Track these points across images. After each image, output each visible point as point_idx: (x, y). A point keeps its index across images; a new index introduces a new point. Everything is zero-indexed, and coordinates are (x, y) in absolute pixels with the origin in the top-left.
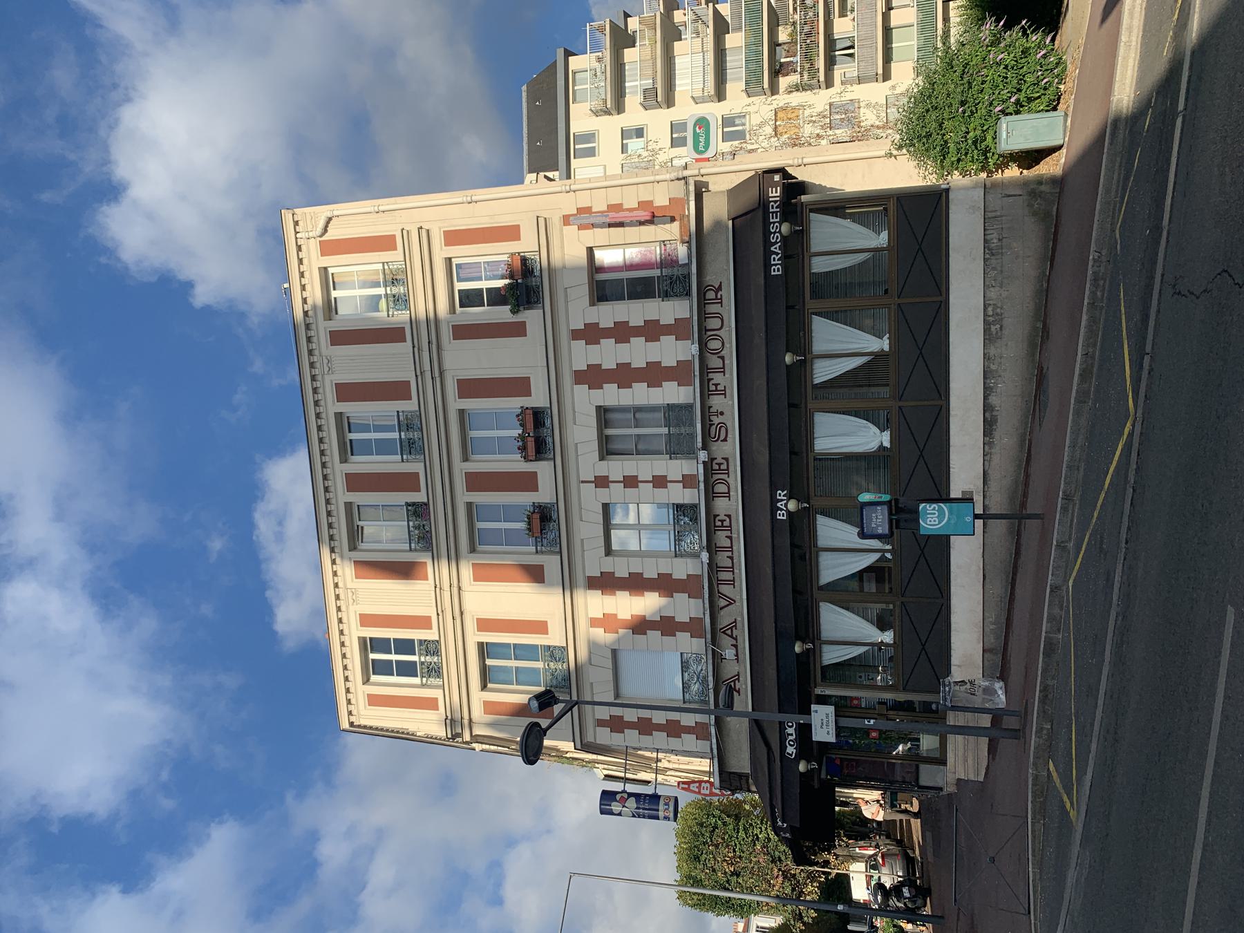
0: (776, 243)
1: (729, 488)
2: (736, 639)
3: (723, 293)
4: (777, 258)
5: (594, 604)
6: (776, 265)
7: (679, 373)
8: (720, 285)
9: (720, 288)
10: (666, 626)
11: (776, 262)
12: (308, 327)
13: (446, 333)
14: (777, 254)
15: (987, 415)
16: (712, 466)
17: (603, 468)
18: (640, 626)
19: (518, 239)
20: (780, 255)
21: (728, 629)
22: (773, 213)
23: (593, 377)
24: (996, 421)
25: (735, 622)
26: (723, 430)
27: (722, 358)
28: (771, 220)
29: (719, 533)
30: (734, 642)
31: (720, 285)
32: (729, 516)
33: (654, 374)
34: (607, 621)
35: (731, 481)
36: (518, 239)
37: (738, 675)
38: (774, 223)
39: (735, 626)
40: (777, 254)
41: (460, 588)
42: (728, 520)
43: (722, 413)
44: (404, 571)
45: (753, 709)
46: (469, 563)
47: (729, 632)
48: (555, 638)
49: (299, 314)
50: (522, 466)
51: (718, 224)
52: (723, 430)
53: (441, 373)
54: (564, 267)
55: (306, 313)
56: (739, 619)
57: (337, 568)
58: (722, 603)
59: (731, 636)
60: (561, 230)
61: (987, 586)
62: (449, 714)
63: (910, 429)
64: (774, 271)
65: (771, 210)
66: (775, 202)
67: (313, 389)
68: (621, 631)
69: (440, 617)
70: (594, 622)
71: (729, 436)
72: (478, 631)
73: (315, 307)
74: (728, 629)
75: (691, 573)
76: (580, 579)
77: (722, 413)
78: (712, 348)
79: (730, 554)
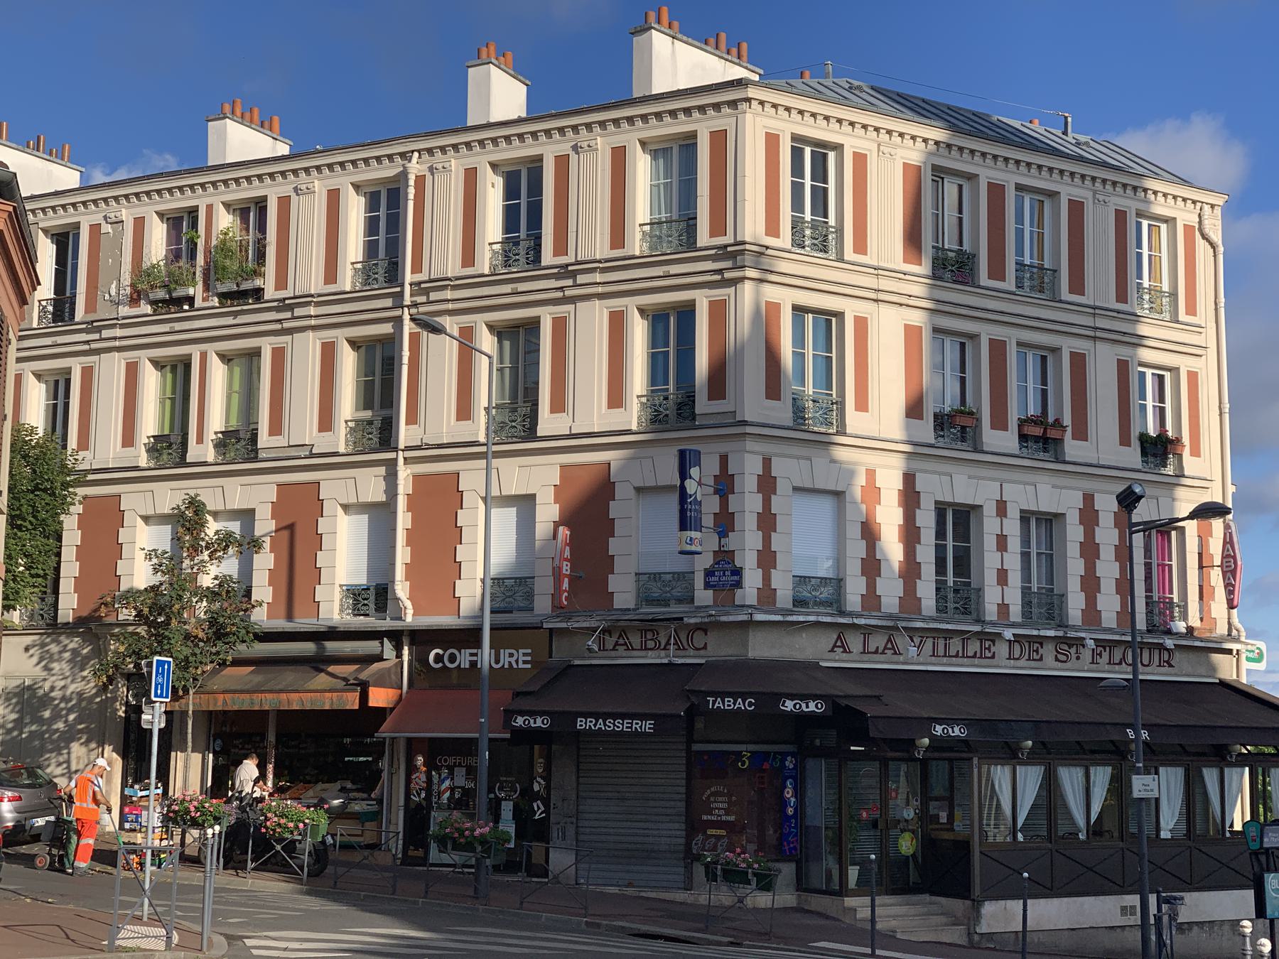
0: (605, 725)
1: (1018, 659)
2: (883, 653)
3: (1166, 669)
4: (637, 726)
5: (890, 481)
6: (586, 723)
7: (1091, 613)
8: (1173, 666)
9: (1171, 666)
10: (872, 566)
11: (588, 724)
12: (1135, 188)
13: (1124, 352)
14: (595, 725)
15: (1186, 926)
16: (988, 640)
17: (1013, 513)
18: (870, 533)
19: (857, 409)
20: (593, 728)
21: (842, 642)
22: (632, 723)
23: (1089, 516)
24: (1182, 934)
25: (900, 654)
26: (1064, 658)
27: (1120, 663)
28: (625, 721)
29: (978, 644)
30: (880, 651)
31: (1173, 666)
32: (993, 657)
33: (1091, 584)
34: (873, 492)
35: (1022, 663)
36: (857, 409)
37: (850, 652)
38: (623, 724)
39: (628, 649)
40: (595, 725)
41: (901, 305)
42: (989, 655)
43: (1078, 658)
44: (913, 238)
45: (1141, 680)
46: (923, 323)
47: (839, 643)
48: (854, 421)
49: (1151, 184)
50: (1014, 416)
51: (1213, 669)
52: (1064, 658)
53: (1095, 338)
54: (1174, 500)
55: (1145, 190)
56: (901, 658)
57: (920, 144)
58: (917, 640)
59: (885, 648)
60: (716, 453)
61: (1066, 932)
62: (769, 252)
63: (1002, 864)
64: (581, 721)
65: (634, 722)
66: (641, 727)
67: (892, 131)
68: (864, 507)
69: (872, 271)
70: (871, 474)
71: (1060, 664)
72: (867, 318)
73: (1148, 202)
74: (842, 642)
75: (923, 603)
76: (918, 464)
77: (1078, 658)
78: (694, 636)
79: (960, 655)
